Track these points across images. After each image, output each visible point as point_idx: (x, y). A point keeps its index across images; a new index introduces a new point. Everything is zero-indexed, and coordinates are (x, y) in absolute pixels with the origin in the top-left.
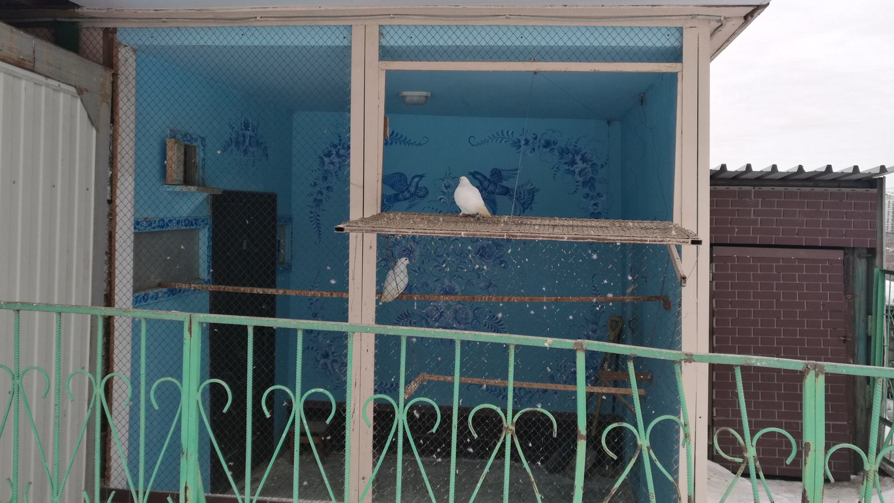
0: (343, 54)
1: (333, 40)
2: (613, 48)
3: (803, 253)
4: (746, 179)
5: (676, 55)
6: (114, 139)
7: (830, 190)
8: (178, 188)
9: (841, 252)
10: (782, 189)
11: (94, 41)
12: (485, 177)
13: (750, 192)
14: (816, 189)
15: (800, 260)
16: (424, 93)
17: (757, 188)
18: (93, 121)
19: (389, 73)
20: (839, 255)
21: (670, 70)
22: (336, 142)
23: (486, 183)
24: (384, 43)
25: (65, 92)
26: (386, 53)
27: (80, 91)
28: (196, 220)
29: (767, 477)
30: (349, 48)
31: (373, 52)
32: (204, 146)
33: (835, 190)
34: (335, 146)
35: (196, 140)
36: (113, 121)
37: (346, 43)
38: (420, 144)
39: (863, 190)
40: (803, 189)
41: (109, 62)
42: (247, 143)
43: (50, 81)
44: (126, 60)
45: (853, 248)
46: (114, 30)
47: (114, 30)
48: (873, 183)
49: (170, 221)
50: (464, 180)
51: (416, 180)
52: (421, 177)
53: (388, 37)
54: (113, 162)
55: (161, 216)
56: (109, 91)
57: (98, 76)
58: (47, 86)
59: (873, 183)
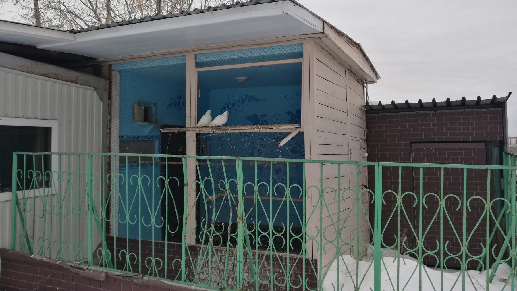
0: (183, 67)
1: (179, 62)
2: (281, 54)
3: (461, 145)
4: (381, 108)
5: (300, 55)
6: (110, 106)
7: (475, 110)
8: (141, 123)
9: (484, 144)
10: (447, 111)
11: (105, 70)
12: (293, 114)
13: (430, 114)
14: (467, 110)
15: (461, 149)
16: (244, 78)
17: (433, 112)
18: (101, 99)
19: (199, 73)
20: (483, 146)
21: (299, 61)
22: (227, 102)
23: (294, 117)
24: (197, 61)
25: (89, 89)
26: (198, 65)
27: (95, 89)
28: (152, 137)
29: (449, 268)
30: (185, 64)
31: (193, 64)
32: (155, 106)
33: (478, 110)
34: (227, 104)
35: (151, 104)
36: (110, 98)
37: (184, 62)
38: (263, 101)
39: (494, 109)
40: (459, 111)
41: (109, 79)
42: (181, 104)
43: (84, 86)
44: (116, 77)
45: (491, 141)
46: (111, 65)
47: (111, 65)
48: (498, 106)
49: (138, 137)
50: (226, 113)
51: (262, 117)
52: (265, 115)
53: (198, 58)
54: (110, 113)
55: (134, 134)
56: (107, 87)
57: (103, 83)
58: (82, 88)
59: (498, 106)
